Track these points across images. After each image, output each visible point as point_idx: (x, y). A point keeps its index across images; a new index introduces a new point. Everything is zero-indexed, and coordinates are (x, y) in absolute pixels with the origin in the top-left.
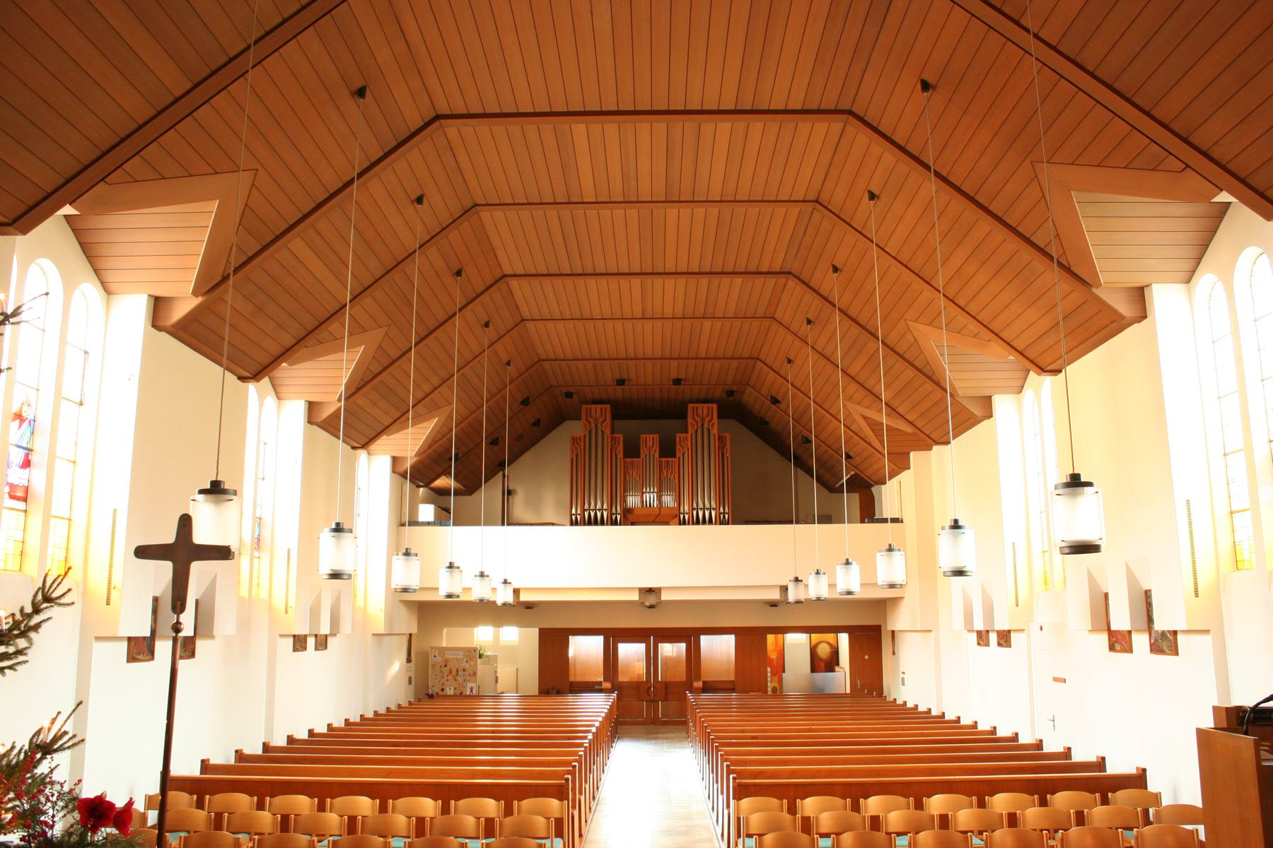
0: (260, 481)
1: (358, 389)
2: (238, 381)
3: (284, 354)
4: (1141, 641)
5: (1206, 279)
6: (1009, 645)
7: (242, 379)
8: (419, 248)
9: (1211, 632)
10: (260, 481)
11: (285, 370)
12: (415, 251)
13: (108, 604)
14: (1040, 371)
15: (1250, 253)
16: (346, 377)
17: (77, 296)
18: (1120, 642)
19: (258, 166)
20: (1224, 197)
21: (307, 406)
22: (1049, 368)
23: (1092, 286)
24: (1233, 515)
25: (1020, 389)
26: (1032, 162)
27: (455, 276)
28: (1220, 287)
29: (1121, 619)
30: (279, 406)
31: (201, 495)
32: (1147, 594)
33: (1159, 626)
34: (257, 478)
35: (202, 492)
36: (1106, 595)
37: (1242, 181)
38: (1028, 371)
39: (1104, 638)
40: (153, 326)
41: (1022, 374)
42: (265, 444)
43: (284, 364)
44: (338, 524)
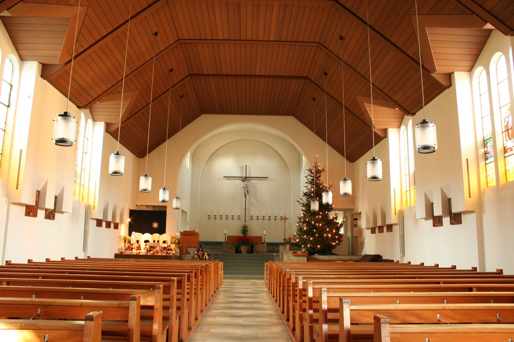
0: (84, 154)
1: (128, 119)
2: (77, 108)
3: (98, 98)
4: (446, 220)
5: (479, 70)
6: (391, 231)
7: (79, 107)
8: (155, 56)
9: (476, 212)
10: (84, 154)
11: (98, 105)
12: (154, 57)
13: (17, 189)
14: (408, 113)
15: (498, 55)
16: (122, 112)
17: (7, 60)
18: (438, 222)
19: (89, 6)
20: (489, 26)
21: (106, 125)
22: (411, 112)
23: (431, 73)
24: (501, 109)
25: (399, 127)
26: (409, 15)
27: (170, 72)
28: (484, 72)
29: (438, 211)
30: (94, 125)
31: (60, 117)
32: (450, 200)
33: (454, 210)
34: (83, 152)
35: (60, 115)
36: (432, 203)
37: (496, 17)
38: (404, 115)
39: (431, 222)
40: (41, 77)
41: (400, 120)
42: (88, 139)
43: (98, 102)
44: (118, 152)
